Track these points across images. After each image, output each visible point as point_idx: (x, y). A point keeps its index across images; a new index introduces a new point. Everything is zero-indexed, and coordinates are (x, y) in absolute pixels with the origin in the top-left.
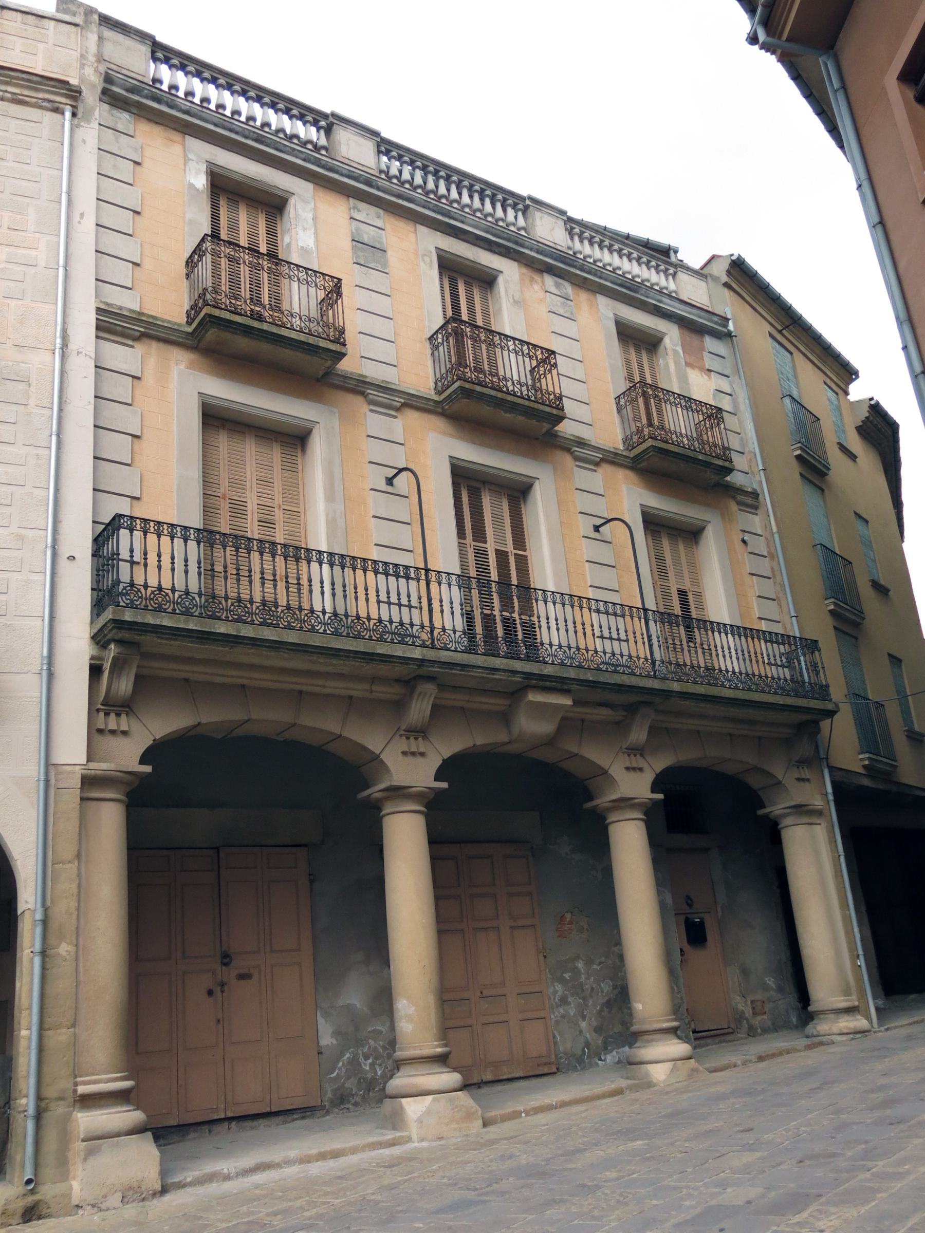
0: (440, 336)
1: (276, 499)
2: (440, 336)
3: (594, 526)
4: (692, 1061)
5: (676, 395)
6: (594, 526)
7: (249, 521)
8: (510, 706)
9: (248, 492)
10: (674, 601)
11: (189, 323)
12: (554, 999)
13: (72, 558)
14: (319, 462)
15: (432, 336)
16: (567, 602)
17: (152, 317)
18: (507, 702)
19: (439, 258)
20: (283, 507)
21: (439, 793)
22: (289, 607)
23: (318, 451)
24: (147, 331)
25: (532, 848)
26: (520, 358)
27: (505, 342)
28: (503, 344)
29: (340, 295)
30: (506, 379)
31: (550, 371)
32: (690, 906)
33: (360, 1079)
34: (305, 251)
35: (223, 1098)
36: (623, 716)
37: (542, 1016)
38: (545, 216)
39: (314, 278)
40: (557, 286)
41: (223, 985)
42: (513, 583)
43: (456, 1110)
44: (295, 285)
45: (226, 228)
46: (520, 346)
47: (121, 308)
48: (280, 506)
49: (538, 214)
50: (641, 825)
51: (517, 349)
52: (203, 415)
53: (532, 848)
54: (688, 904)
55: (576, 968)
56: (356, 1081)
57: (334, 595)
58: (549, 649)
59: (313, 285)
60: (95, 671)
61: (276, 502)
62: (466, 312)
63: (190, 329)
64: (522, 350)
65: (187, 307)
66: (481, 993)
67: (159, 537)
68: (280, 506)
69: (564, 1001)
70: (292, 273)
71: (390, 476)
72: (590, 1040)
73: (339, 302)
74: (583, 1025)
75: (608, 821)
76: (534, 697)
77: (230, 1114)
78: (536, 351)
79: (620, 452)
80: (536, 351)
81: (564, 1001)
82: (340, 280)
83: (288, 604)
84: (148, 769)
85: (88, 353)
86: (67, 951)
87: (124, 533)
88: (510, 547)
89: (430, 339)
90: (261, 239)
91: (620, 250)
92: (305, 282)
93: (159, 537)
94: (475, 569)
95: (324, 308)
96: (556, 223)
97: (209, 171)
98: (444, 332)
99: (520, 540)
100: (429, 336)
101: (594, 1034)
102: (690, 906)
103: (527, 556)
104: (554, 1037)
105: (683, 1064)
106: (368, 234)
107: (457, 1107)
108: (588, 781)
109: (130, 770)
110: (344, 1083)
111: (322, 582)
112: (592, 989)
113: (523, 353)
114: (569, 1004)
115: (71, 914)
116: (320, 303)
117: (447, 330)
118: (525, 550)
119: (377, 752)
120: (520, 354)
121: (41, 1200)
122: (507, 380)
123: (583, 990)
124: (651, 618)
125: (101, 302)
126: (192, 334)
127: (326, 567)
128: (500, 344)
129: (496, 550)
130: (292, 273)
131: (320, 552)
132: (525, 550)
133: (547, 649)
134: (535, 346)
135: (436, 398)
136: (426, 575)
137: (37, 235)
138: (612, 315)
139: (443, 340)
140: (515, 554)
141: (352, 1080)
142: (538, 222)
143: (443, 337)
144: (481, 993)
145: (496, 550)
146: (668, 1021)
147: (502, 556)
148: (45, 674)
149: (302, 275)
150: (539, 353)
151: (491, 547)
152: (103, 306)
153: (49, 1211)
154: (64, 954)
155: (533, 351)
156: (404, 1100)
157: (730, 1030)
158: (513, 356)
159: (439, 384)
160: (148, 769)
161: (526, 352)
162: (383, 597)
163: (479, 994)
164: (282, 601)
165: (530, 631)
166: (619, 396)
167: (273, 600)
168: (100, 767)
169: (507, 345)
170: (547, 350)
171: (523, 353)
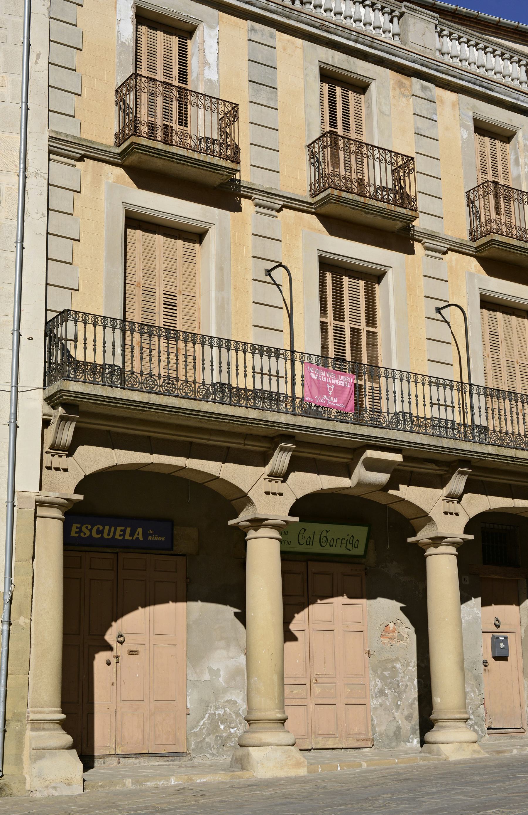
0: (317, 146)
1: (178, 285)
2: (317, 146)
3: (436, 308)
4: (476, 745)
5: (520, 192)
6: (436, 308)
7: (156, 305)
8: (352, 459)
9: (156, 281)
10: (502, 372)
11: (118, 145)
12: (374, 690)
13: (31, 339)
14: (213, 242)
15: (311, 144)
16: (405, 378)
17: (90, 142)
18: (350, 456)
19: (321, 69)
20: (183, 293)
21: (466, 541)
22: (186, 381)
23: (213, 242)
24: (86, 153)
25: (366, 569)
26: (383, 165)
27: (371, 151)
28: (369, 154)
29: (236, 118)
30: (369, 185)
31: (409, 174)
32: (498, 626)
33: (217, 737)
34: (209, 82)
35: (114, 740)
36: (445, 470)
37: (333, 682)
38: (418, 21)
39: (216, 105)
40: (423, 88)
41: (117, 657)
42: (363, 362)
43: (289, 759)
44: (201, 112)
45: (147, 54)
46: (384, 155)
47: (67, 135)
48: (180, 292)
49: (411, 20)
50: (455, 558)
51: (381, 157)
52: (126, 217)
53: (366, 569)
54: (496, 626)
55: (395, 667)
56: (214, 738)
57: (220, 371)
58: (387, 416)
59: (216, 111)
60: (46, 423)
61: (178, 288)
62: (342, 116)
63: (118, 150)
64: (385, 158)
65: (115, 129)
66: (316, 680)
67: (95, 327)
68: (180, 292)
69: (382, 693)
70: (199, 102)
71: (269, 268)
72: (401, 725)
73: (236, 123)
74: (397, 714)
75: (427, 553)
76: (370, 453)
77: (119, 751)
78: (397, 158)
79: (465, 243)
80: (397, 158)
81: (382, 693)
82: (237, 105)
83: (186, 379)
84: (80, 497)
85: (42, 174)
86: (24, 622)
87: (71, 324)
88: (363, 326)
89: (308, 146)
90: (173, 61)
91: (486, 47)
92: (209, 110)
93: (95, 327)
94: (333, 343)
95: (223, 125)
96: (427, 27)
97: (135, 7)
98: (320, 143)
99: (371, 320)
100: (308, 144)
101: (405, 721)
102: (498, 626)
103: (376, 333)
104: (372, 720)
105: (468, 746)
106: (262, 53)
107: (289, 757)
108: (412, 521)
109: (68, 497)
110: (204, 739)
111: (212, 362)
112: (407, 686)
113: (386, 161)
114: (386, 695)
115: (27, 597)
116: (220, 120)
117: (323, 142)
118: (376, 327)
119: (246, 491)
120: (384, 162)
121: (5, 785)
122: (370, 186)
123: (398, 686)
124: (475, 391)
125: (53, 131)
126: (120, 154)
127: (215, 349)
128: (367, 154)
129: (351, 328)
130: (199, 102)
131: (211, 337)
132: (376, 327)
133: (385, 417)
134: (397, 153)
135: (310, 200)
136: (292, 355)
137: (5, 75)
138: (471, 114)
139: (319, 150)
140: (367, 331)
141: (211, 736)
142: (411, 28)
143: (319, 147)
144: (316, 680)
145: (351, 328)
146: (461, 712)
147: (355, 333)
148: (12, 426)
149: (208, 104)
150: (399, 160)
151: (347, 325)
152: (53, 135)
153: (11, 791)
154: (23, 624)
155: (395, 158)
156: (250, 748)
157: (522, 730)
158: (377, 164)
159: (313, 187)
160: (80, 497)
161: (389, 159)
162: (258, 369)
163: (314, 681)
164: (182, 377)
165: (376, 398)
166: (470, 191)
167: (175, 376)
168: (48, 495)
169: (373, 154)
170: (407, 156)
171: (386, 161)
